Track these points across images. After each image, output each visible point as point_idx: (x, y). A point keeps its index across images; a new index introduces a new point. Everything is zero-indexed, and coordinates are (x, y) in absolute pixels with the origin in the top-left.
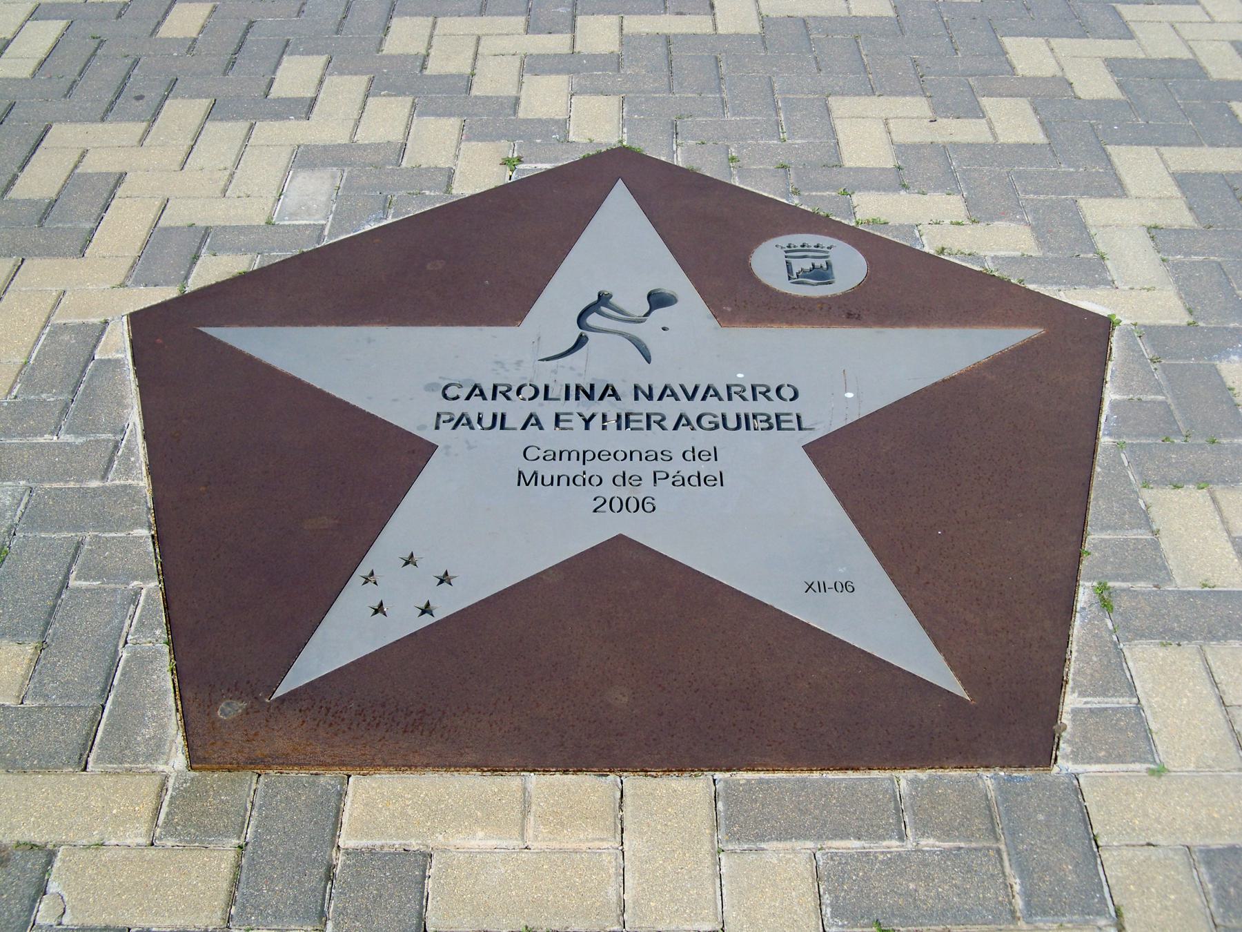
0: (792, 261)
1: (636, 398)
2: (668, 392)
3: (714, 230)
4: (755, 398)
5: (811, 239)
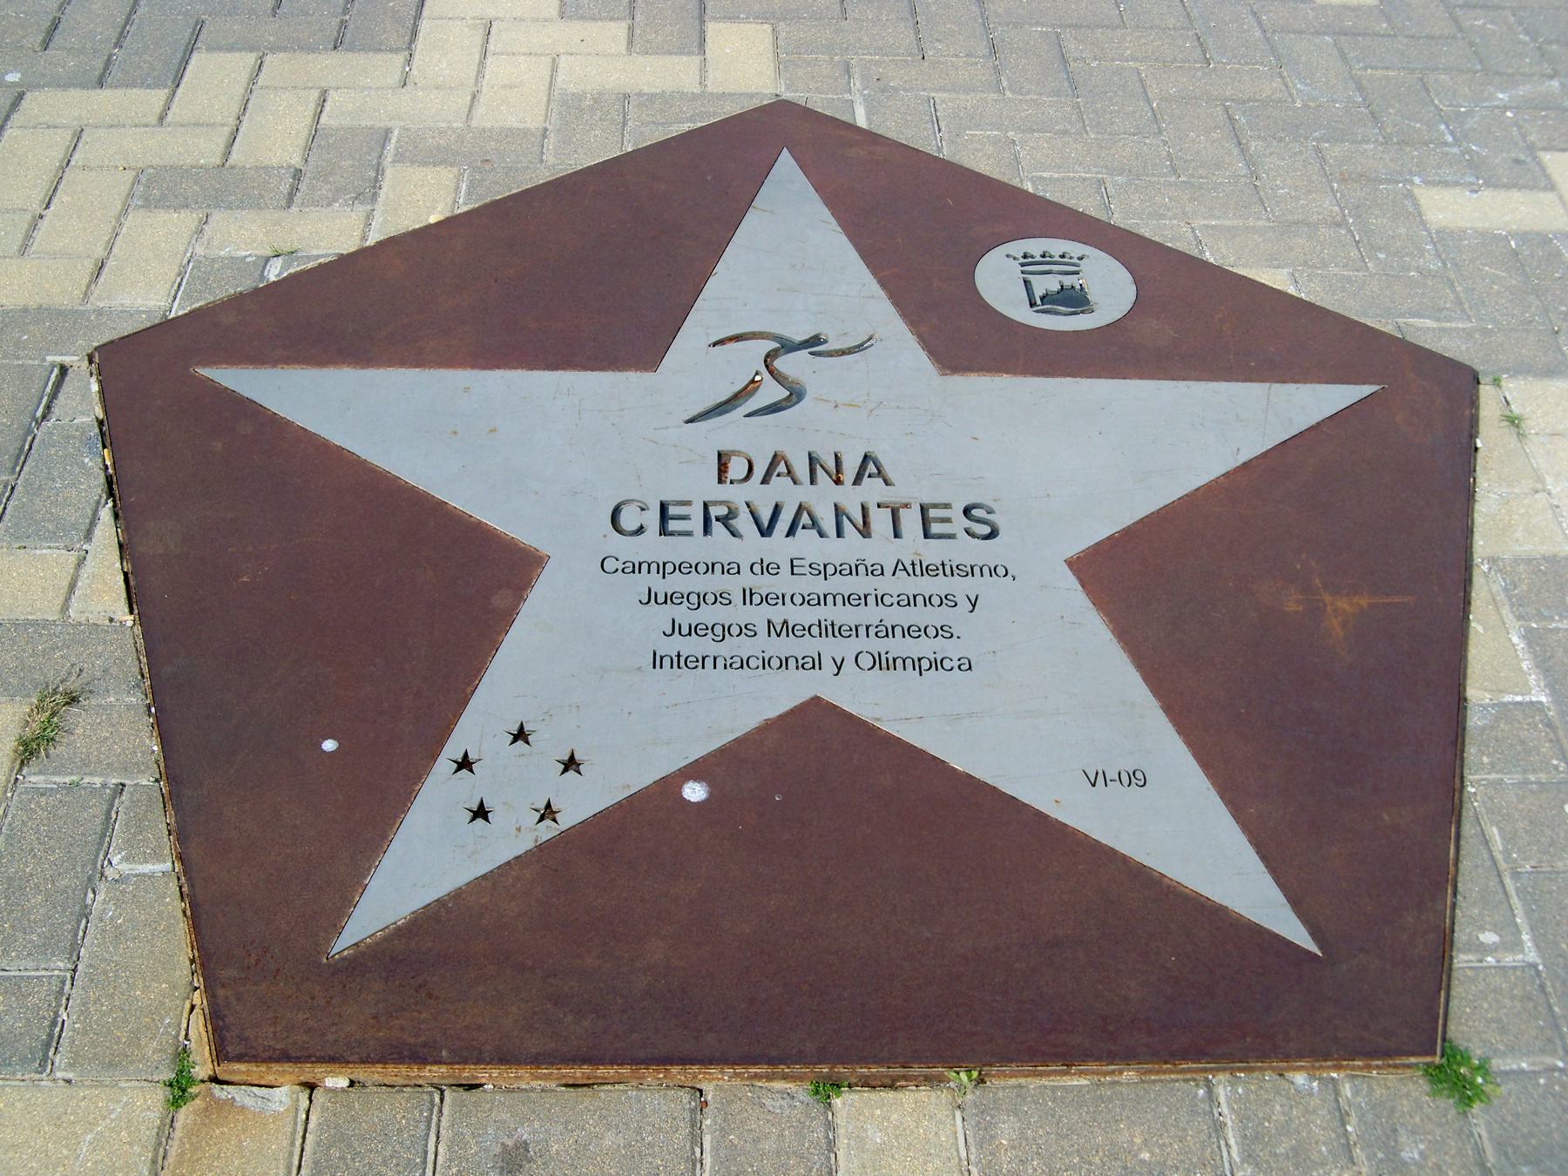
3: (926, 229)
5: (1056, 246)
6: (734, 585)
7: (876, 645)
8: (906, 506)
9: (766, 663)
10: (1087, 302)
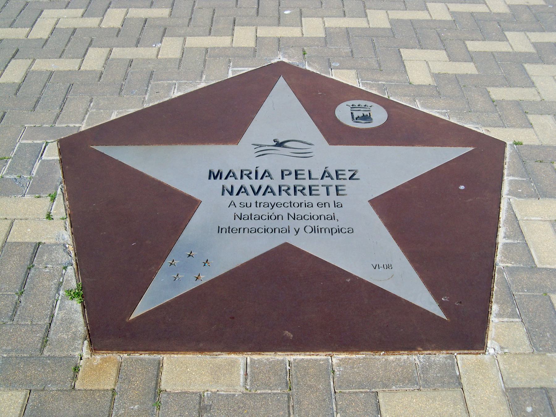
0: (355, 113)
2: (243, 190)
3: (319, 96)
4: (295, 194)
5: (363, 103)
7: (313, 223)
8: (331, 186)
9: (266, 230)
10: (372, 119)
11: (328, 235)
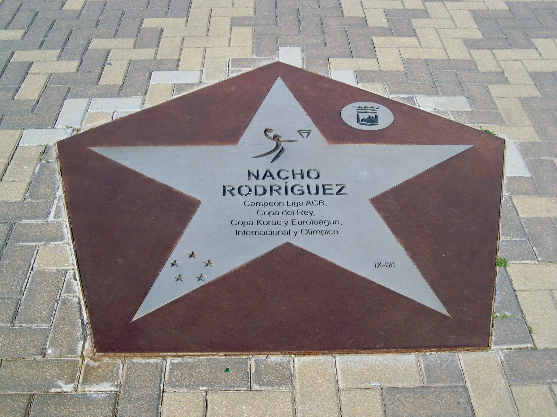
0: (359, 114)
1: (258, 171)
3: (323, 100)
5: (369, 104)
6: (280, 209)
11: (319, 235)
